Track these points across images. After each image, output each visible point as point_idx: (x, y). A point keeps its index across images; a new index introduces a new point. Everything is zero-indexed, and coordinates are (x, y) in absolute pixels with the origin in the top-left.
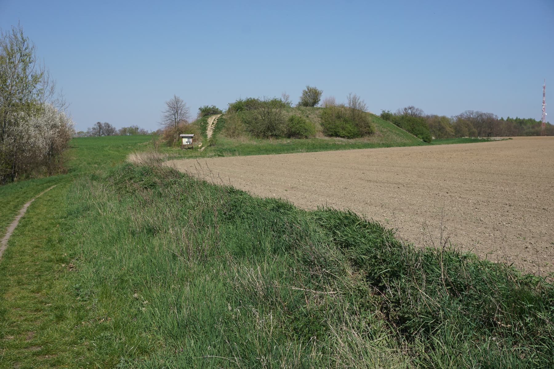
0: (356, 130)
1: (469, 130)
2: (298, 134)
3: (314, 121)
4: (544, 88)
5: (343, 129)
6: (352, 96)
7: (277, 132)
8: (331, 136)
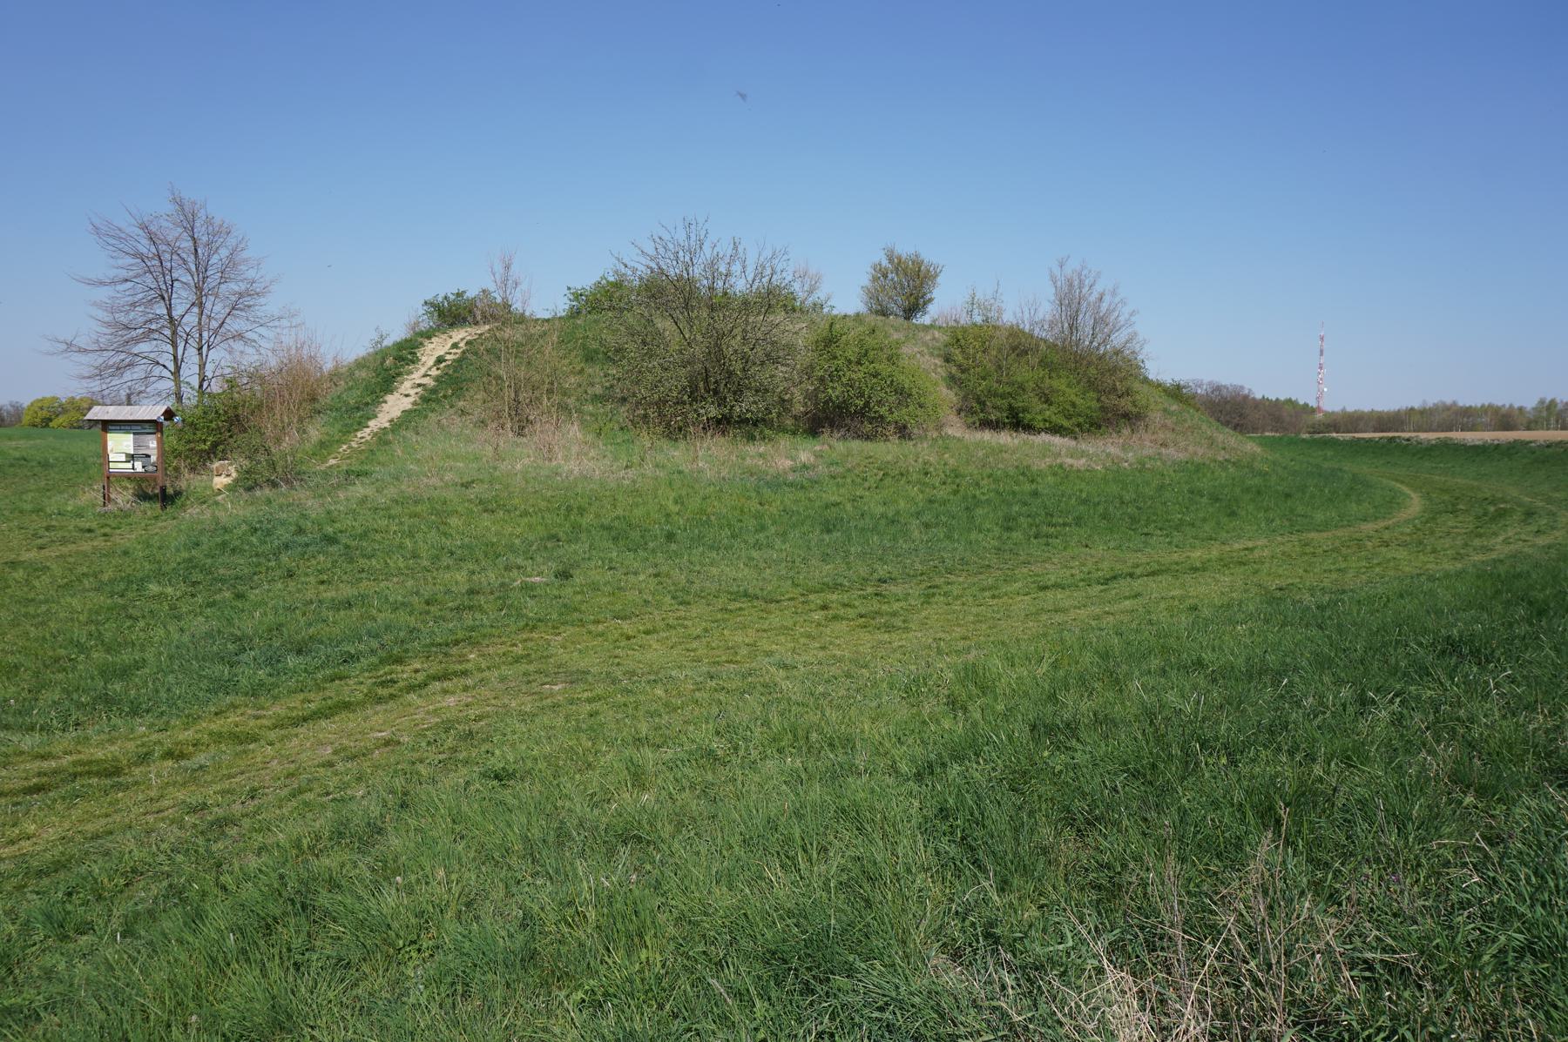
2: (862, 413)
3: (922, 364)
4: (1322, 339)
6: (1072, 267)
7: (747, 405)
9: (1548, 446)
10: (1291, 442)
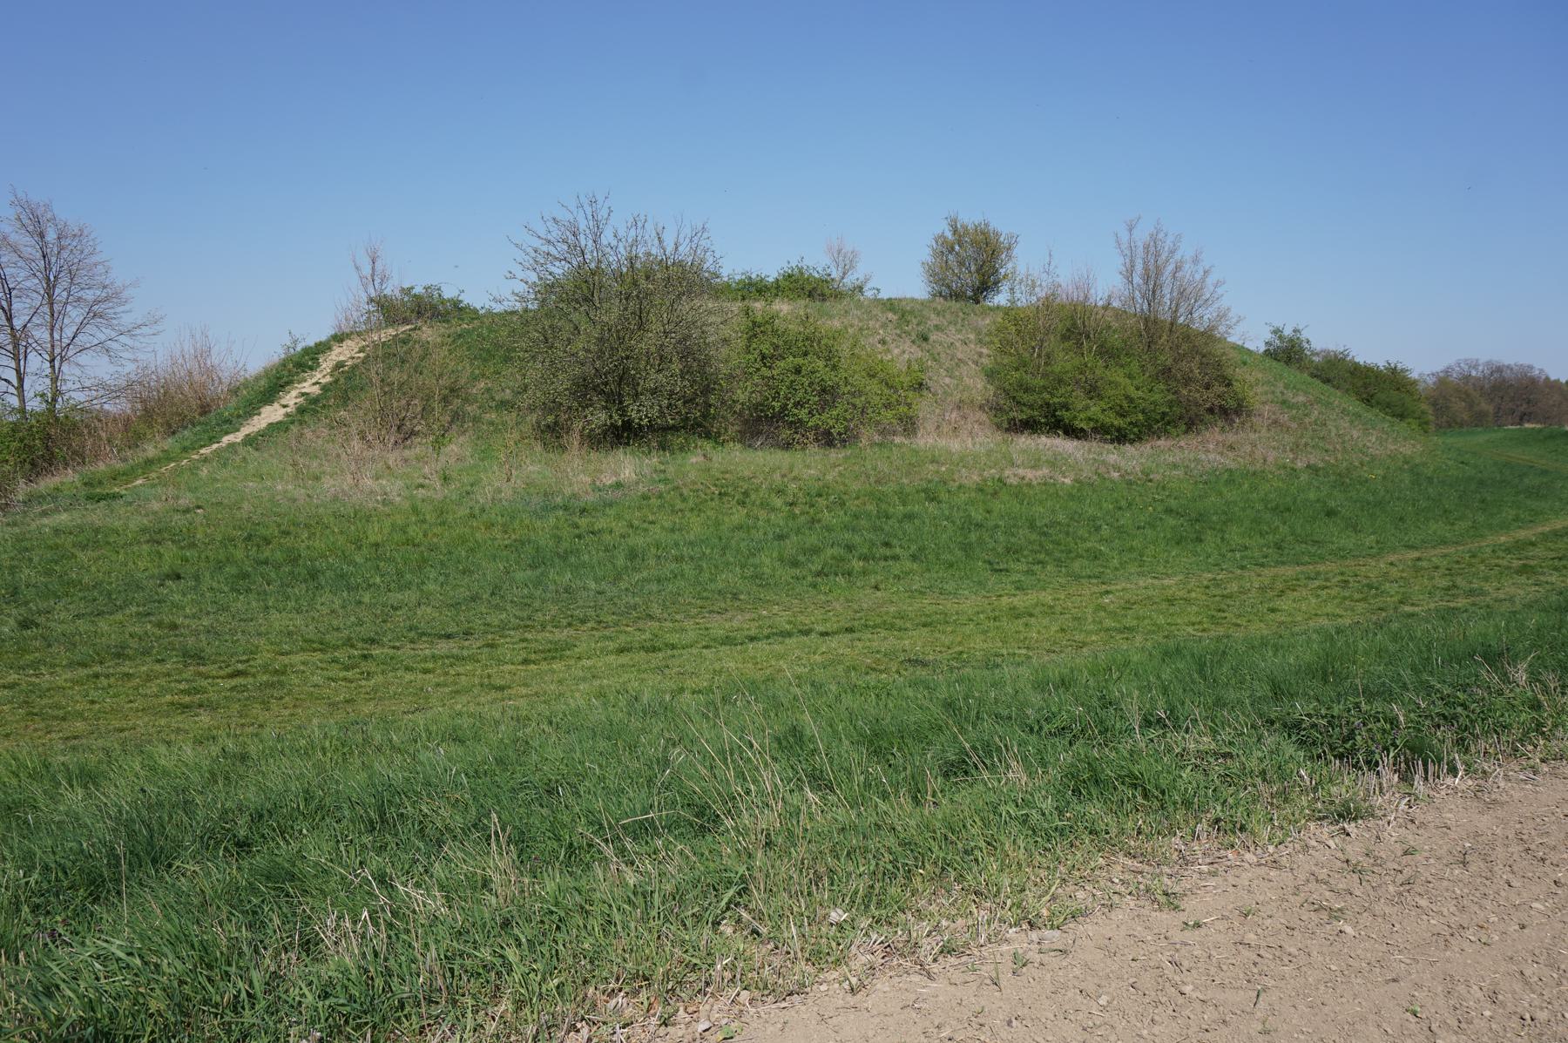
0: (1160, 396)
1: (1471, 406)
5: (1093, 391)
6: (1142, 235)
8: (1029, 426)
10: (1552, 437)
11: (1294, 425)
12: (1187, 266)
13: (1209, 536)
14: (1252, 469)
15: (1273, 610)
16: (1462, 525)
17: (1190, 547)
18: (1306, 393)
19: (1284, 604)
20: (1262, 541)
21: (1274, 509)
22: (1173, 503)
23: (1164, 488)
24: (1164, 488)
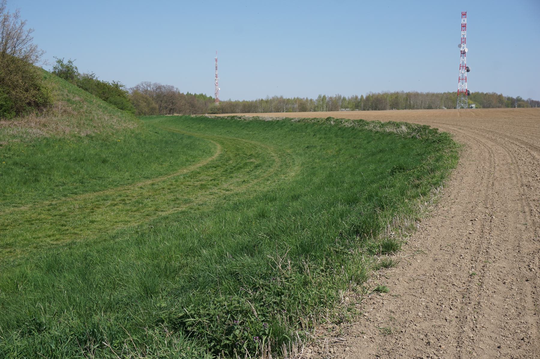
4: (216, 60)
9: (299, 121)
11: (76, 113)
12: (11, 19)
13: (42, 177)
14: (58, 137)
15: (92, 222)
16: (167, 164)
17: (33, 185)
18: (79, 96)
19: (97, 217)
20: (73, 179)
21: (75, 160)
22: (17, 159)
23: (9, 150)
24: (9, 150)
